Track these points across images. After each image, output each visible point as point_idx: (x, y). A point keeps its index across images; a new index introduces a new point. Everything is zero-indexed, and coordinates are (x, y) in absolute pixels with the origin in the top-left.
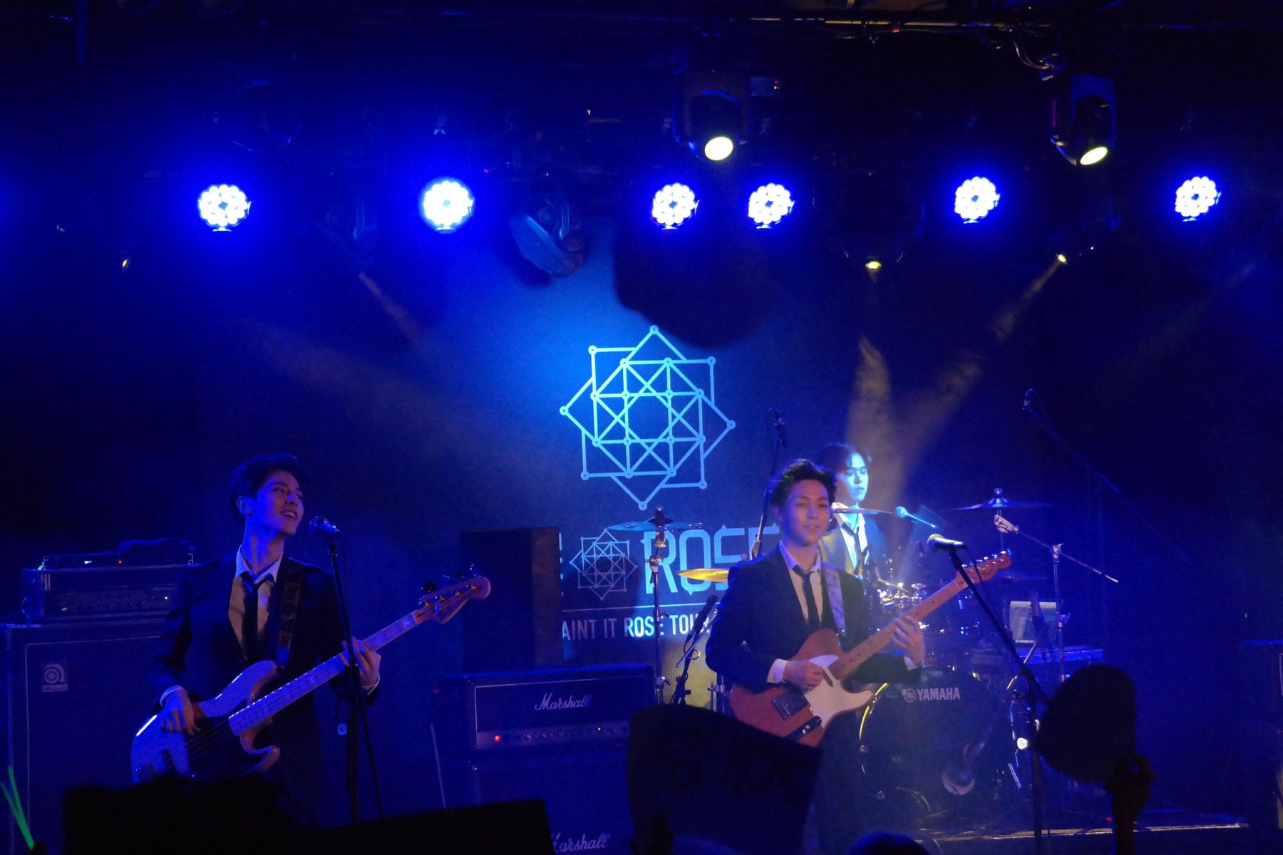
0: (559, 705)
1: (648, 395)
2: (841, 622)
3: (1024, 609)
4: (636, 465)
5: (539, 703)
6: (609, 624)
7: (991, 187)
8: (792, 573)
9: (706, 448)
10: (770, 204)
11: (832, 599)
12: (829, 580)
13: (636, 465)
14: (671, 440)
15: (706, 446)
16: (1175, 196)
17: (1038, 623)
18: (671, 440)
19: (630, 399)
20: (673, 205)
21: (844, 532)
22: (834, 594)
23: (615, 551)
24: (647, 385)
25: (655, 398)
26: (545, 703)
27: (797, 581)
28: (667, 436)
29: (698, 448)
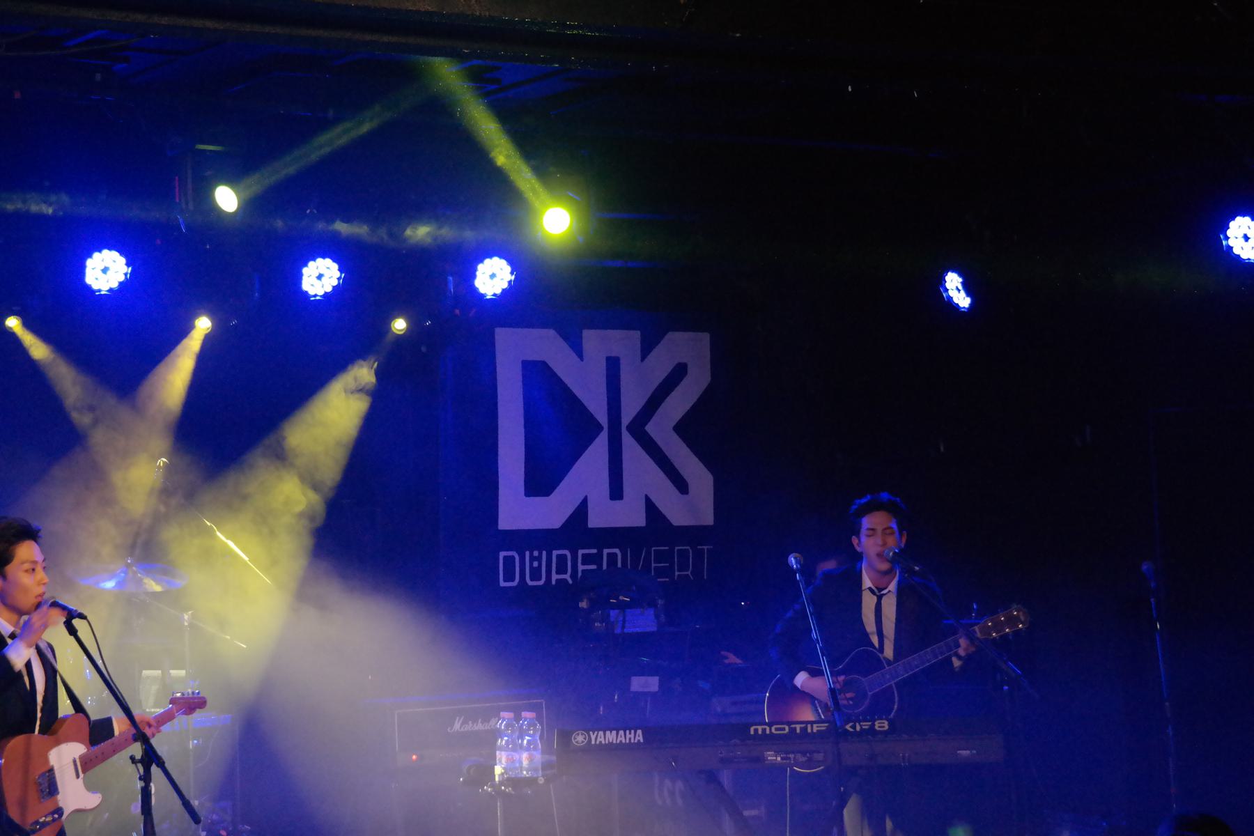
0: (470, 727)
5: (452, 725)
26: (457, 726)
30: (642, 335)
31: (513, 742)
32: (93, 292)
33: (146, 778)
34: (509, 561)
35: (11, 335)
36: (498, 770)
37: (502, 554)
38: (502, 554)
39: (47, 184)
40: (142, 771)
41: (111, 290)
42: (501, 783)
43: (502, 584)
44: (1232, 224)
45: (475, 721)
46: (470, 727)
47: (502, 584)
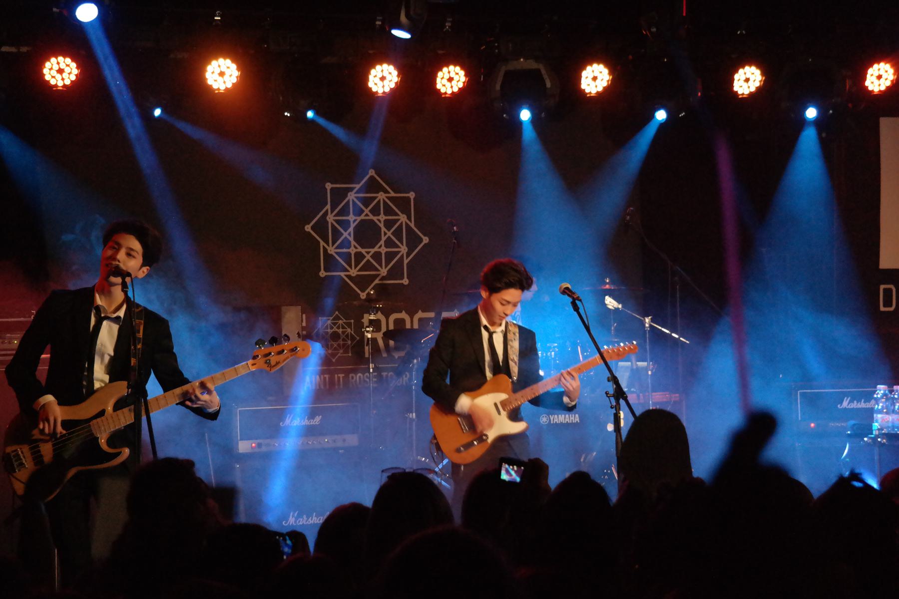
0: (855, 405)
1: (367, 218)
2: (514, 369)
3: (627, 367)
4: (355, 200)
5: (841, 403)
6: (339, 378)
7: (606, 71)
8: (483, 329)
9: (408, 256)
10: (451, 79)
11: (510, 352)
12: (510, 336)
13: (355, 200)
14: (383, 250)
15: (408, 255)
16: (733, 80)
17: (636, 373)
18: (383, 250)
19: (355, 221)
20: (383, 78)
21: (483, 329)
22: (512, 347)
23: (343, 327)
24: (368, 257)
25: (373, 247)
26: (845, 404)
27: (485, 335)
28: (380, 247)
29: (406, 224)
30: (883, 116)
31: (887, 408)
32: (214, 90)
33: (617, 408)
34: (888, 292)
35: (518, 124)
36: (876, 426)
37: (882, 287)
38: (882, 287)
39: (824, 135)
40: (614, 404)
41: (598, 93)
42: (877, 436)
43: (882, 309)
44: (870, 88)
45: (859, 401)
46: (855, 405)
47: (882, 309)
